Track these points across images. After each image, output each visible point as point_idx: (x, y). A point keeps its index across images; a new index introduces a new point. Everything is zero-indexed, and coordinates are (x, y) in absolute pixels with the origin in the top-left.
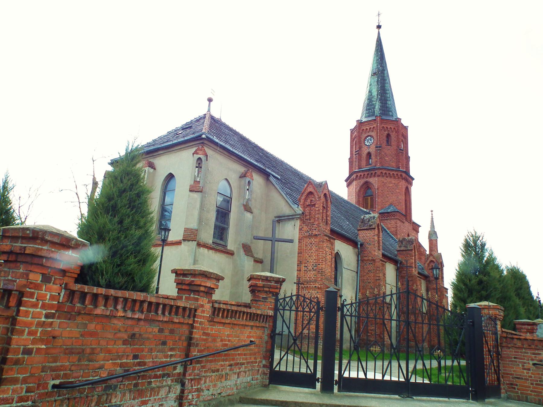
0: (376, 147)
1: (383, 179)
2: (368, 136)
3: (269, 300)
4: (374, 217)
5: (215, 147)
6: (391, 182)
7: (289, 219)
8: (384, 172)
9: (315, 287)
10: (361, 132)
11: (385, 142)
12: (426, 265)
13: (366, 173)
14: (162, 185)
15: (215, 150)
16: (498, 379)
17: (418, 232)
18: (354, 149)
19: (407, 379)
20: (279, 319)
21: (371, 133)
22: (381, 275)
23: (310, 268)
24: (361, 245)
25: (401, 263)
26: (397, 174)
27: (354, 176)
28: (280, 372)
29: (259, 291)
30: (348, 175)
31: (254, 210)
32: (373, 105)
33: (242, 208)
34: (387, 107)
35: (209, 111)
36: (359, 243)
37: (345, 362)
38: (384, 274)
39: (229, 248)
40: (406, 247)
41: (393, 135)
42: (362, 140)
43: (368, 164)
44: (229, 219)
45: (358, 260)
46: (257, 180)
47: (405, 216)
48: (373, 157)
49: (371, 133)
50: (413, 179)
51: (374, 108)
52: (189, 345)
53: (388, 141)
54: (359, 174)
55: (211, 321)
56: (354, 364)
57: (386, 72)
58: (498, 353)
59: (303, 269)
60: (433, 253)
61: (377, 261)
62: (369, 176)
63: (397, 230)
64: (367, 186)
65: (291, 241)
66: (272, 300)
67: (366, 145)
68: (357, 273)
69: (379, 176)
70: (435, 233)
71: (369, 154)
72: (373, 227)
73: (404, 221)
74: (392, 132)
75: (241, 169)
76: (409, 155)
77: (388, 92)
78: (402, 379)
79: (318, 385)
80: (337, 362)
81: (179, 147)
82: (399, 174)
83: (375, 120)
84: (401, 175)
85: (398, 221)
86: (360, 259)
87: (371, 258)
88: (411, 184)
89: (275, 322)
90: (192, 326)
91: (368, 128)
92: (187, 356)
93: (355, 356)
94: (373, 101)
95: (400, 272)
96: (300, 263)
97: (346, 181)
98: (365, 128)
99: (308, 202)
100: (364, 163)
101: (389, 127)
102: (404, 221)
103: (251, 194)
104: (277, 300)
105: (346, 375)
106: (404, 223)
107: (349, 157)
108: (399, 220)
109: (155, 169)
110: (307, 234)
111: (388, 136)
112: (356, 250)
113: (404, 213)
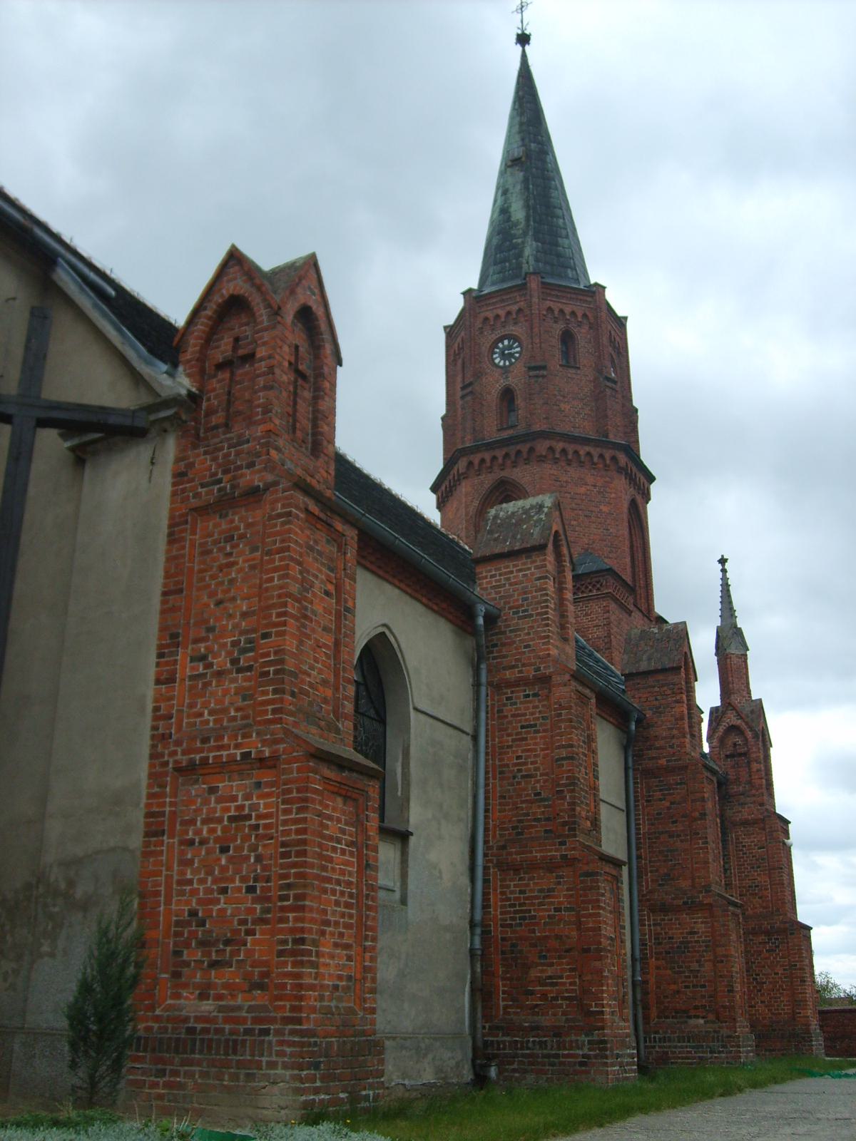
2: (501, 339)
4: (541, 506)
8: (559, 446)
9: (246, 756)
10: (478, 324)
11: (558, 354)
13: (499, 453)
18: (459, 379)
23: (221, 661)
25: (638, 722)
26: (601, 456)
27: (462, 465)
30: (439, 466)
32: (515, 246)
34: (559, 255)
36: (481, 609)
41: (582, 335)
45: (477, 685)
48: (520, 402)
51: (520, 255)
54: (476, 459)
57: (549, 158)
59: (185, 667)
60: (736, 699)
61: (557, 679)
62: (508, 462)
63: (609, 635)
67: (497, 366)
68: (475, 738)
70: (739, 633)
73: (631, 607)
74: (580, 324)
76: (635, 404)
77: (559, 212)
82: (608, 454)
83: (523, 287)
84: (614, 458)
85: (613, 606)
86: (484, 679)
87: (530, 672)
91: (502, 313)
94: (514, 236)
95: (638, 756)
96: (171, 641)
99: (223, 349)
101: (567, 310)
102: (631, 607)
106: (630, 613)
107: (443, 412)
108: (616, 600)
110: (208, 495)
111: (567, 338)
113: (629, 580)
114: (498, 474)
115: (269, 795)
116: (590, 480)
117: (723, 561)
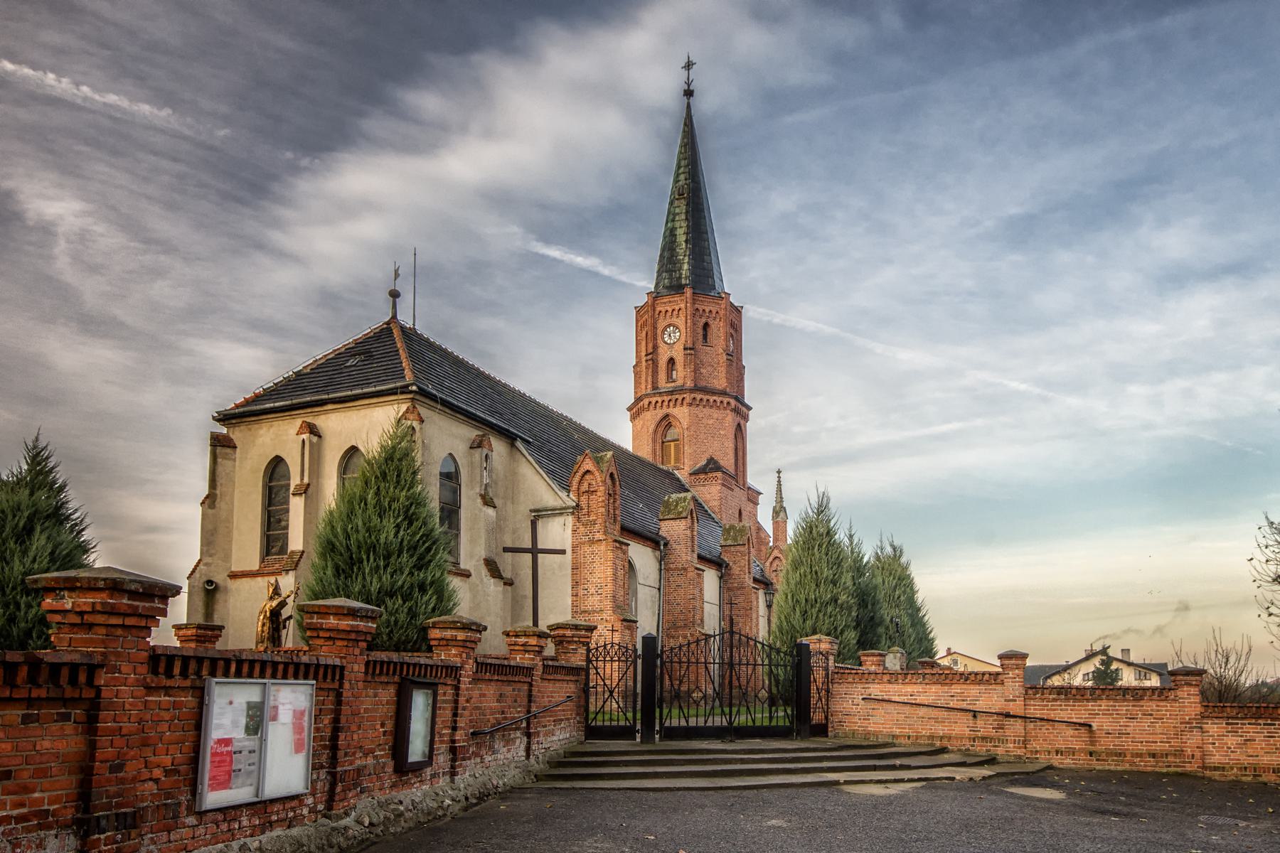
0: (685, 349)
1: (694, 410)
2: (669, 326)
3: (580, 651)
5: (432, 403)
6: (710, 417)
7: (555, 515)
8: (699, 396)
12: (768, 564)
14: (340, 465)
15: (431, 408)
16: (826, 718)
17: (756, 504)
19: (730, 723)
20: (592, 671)
21: (675, 320)
22: (697, 592)
24: (666, 545)
28: (597, 728)
29: (569, 642)
31: (497, 502)
33: (479, 500)
35: (394, 317)
37: (665, 711)
38: (701, 590)
39: (462, 566)
40: (735, 540)
41: (719, 330)
42: (659, 332)
43: (669, 378)
44: (458, 520)
45: (660, 570)
46: (498, 447)
47: (735, 478)
49: (675, 320)
50: (749, 408)
51: (681, 268)
52: (530, 701)
53: (705, 337)
55: (476, 680)
56: (675, 712)
58: (828, 691)
59: (581, 592)
64: (666, 423)
65: (563, 552)
66: (583, 650)
69: (690, 405)
71: (671, 361)
72: (684, 515)
75: (472, 433)
78: (725, 724)
79: (638, 736)
80: (658, 711)
81: (367, 401)
88: (746, 418)
89: (588, 675)
90: (531, 685)
92: (529, 712)
93: (676, 704)
96: (576, 584)
97: (629, 409)
98: (663, 310)
99: (585, 487)
100: (662, 376)
103: (490, 477)
104: (589, 650)
105: (667, 724)
109: (320, 436)
112: (658, 553)
113: (732, 470)
114: (665, 411)
115: (738, 712)
116: (715, 416)
117: (779, 472)
